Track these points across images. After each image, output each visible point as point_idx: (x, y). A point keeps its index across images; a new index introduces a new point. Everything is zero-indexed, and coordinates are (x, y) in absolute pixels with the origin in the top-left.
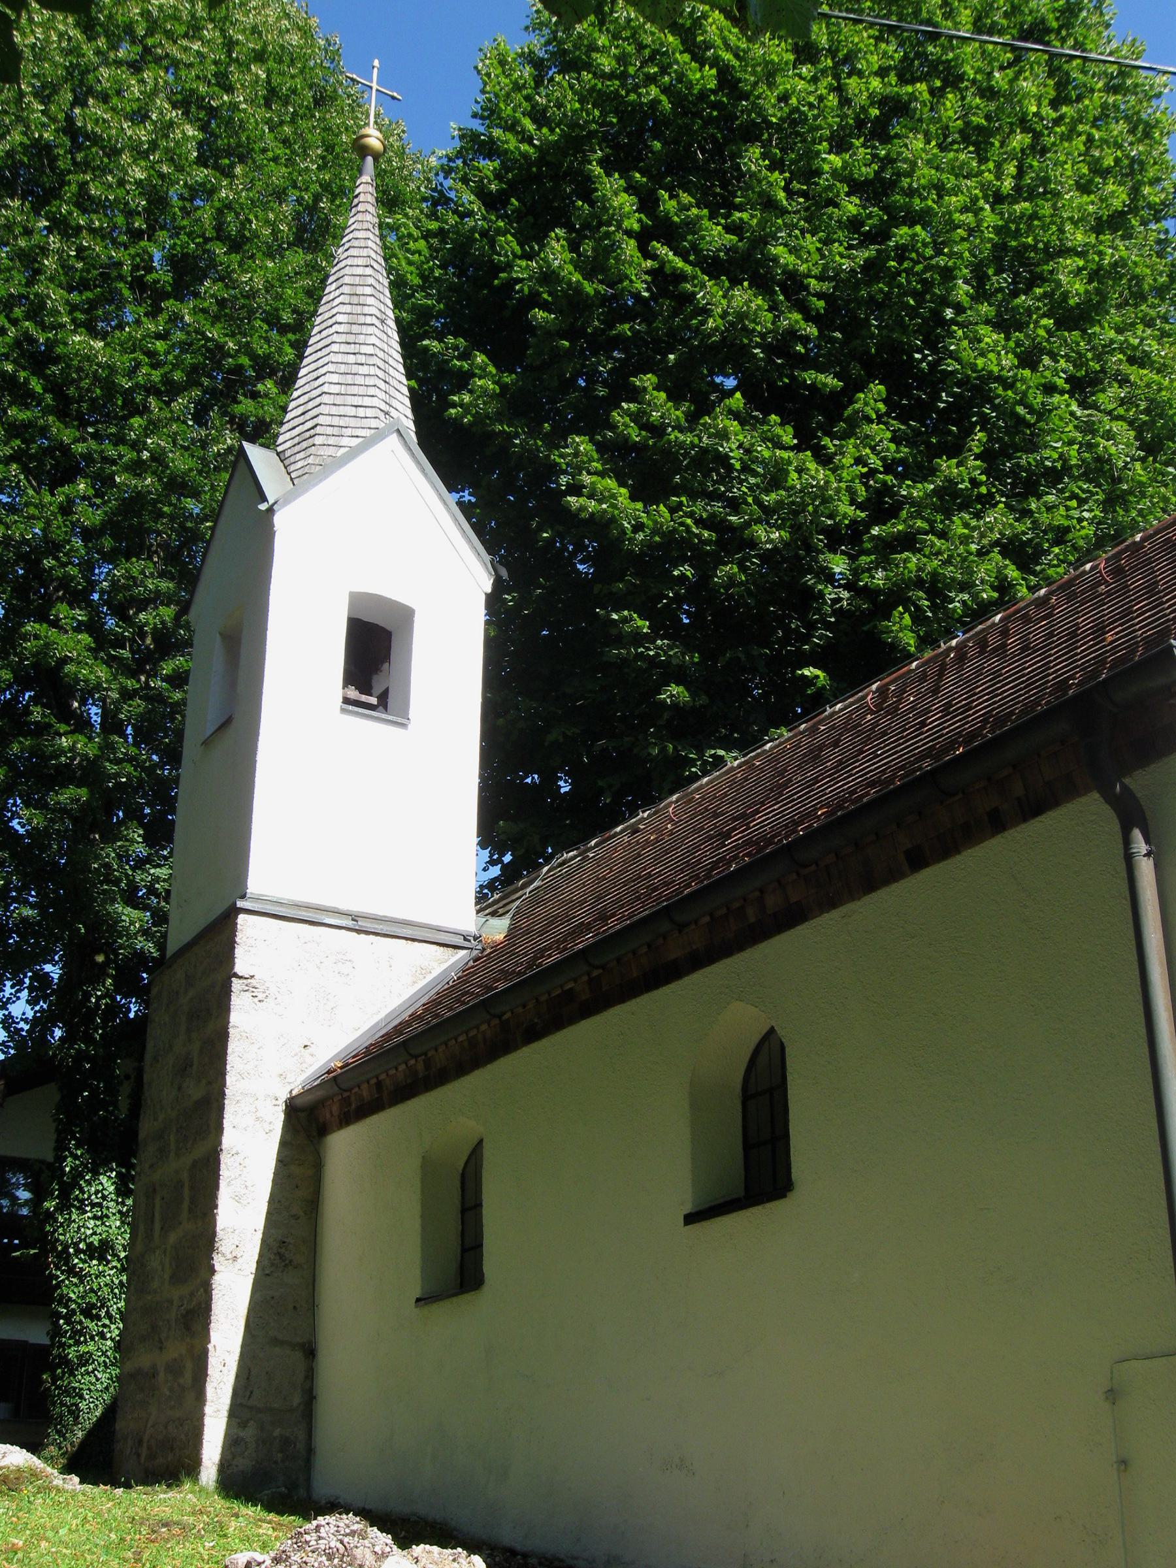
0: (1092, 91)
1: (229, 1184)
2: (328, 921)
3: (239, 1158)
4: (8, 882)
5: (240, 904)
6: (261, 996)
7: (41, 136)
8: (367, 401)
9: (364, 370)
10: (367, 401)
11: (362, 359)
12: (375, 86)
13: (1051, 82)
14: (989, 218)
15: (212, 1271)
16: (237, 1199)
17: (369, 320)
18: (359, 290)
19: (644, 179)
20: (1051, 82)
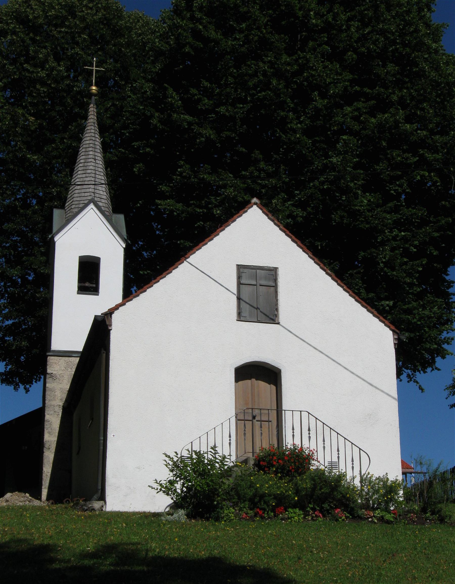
0: (188, 37)
1: (47, 429)
2: (74, 355)
3: (50, 422)
4: (395, 1)
5: (48, 354)
6: (55, 378)
7: (14, 77)
8: (88, 190)
9: (88, 179)
10: (88, 190)
11: (87, 175)
12: (94, 68)
13: (169, 22)
14: (206, 477)
15: (43, 452)
16: (49, 433)
17: (90, 160)
18: (88, 149)
19: (29, 156)
20: (169, 22)
